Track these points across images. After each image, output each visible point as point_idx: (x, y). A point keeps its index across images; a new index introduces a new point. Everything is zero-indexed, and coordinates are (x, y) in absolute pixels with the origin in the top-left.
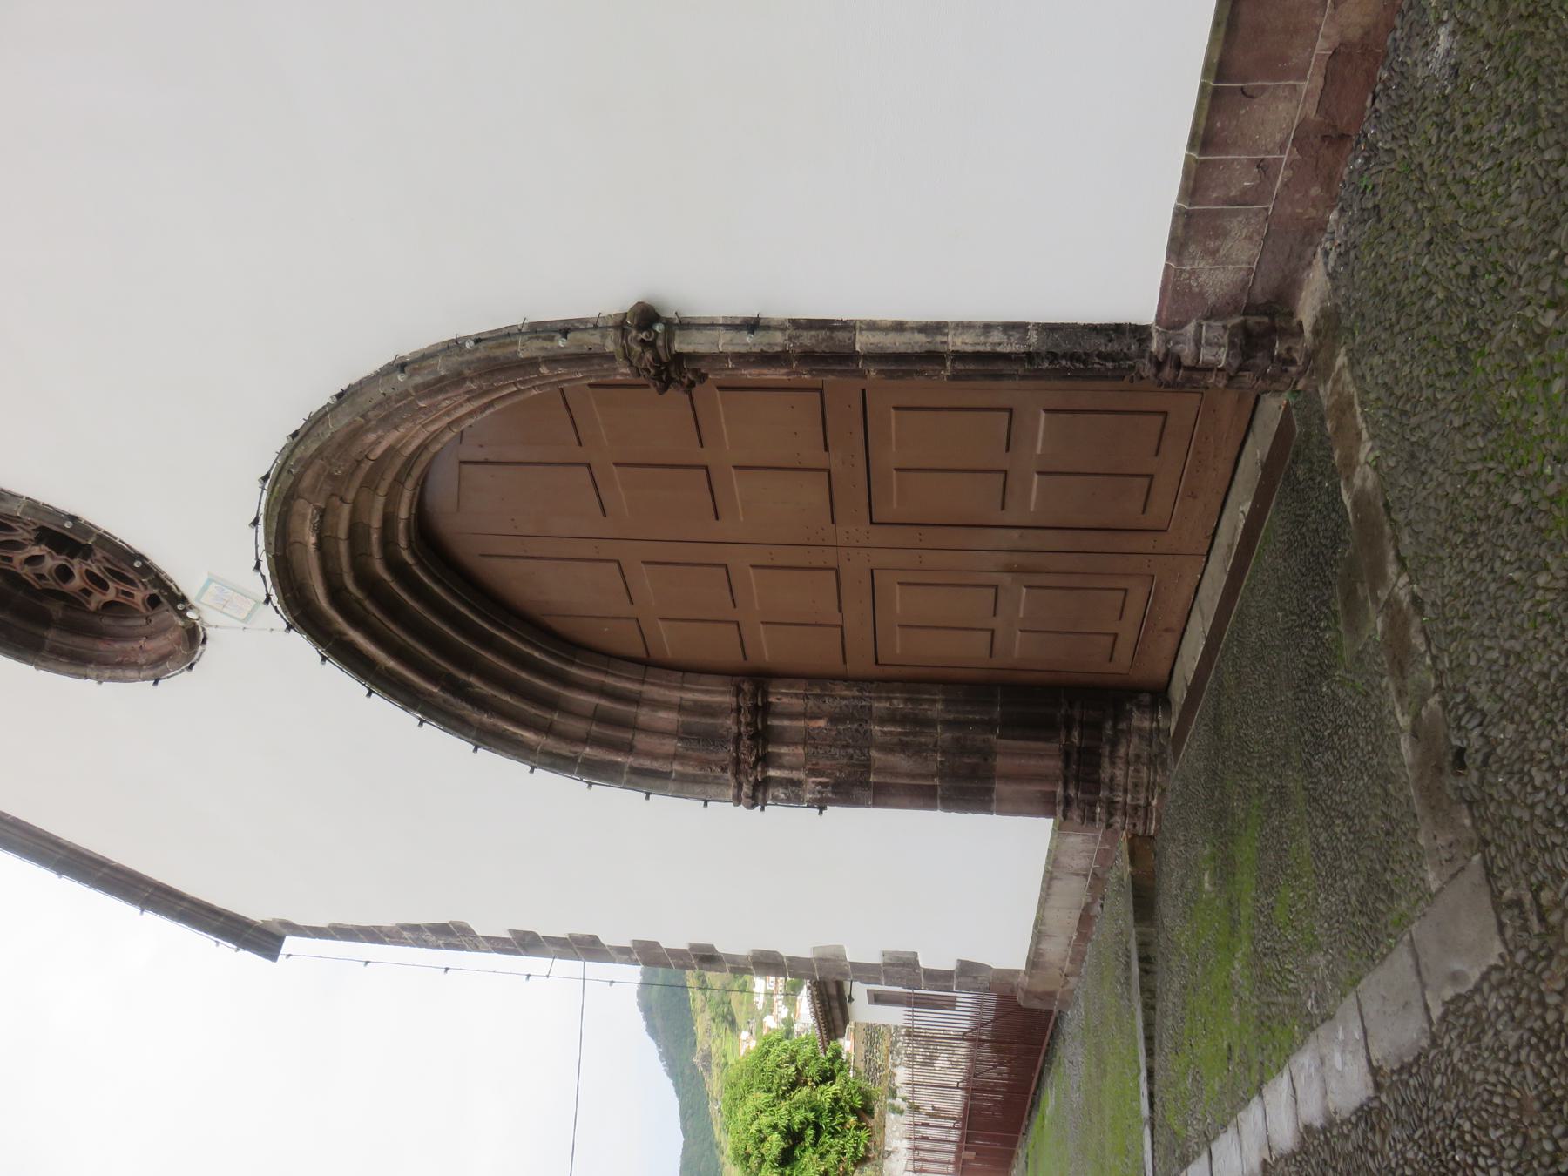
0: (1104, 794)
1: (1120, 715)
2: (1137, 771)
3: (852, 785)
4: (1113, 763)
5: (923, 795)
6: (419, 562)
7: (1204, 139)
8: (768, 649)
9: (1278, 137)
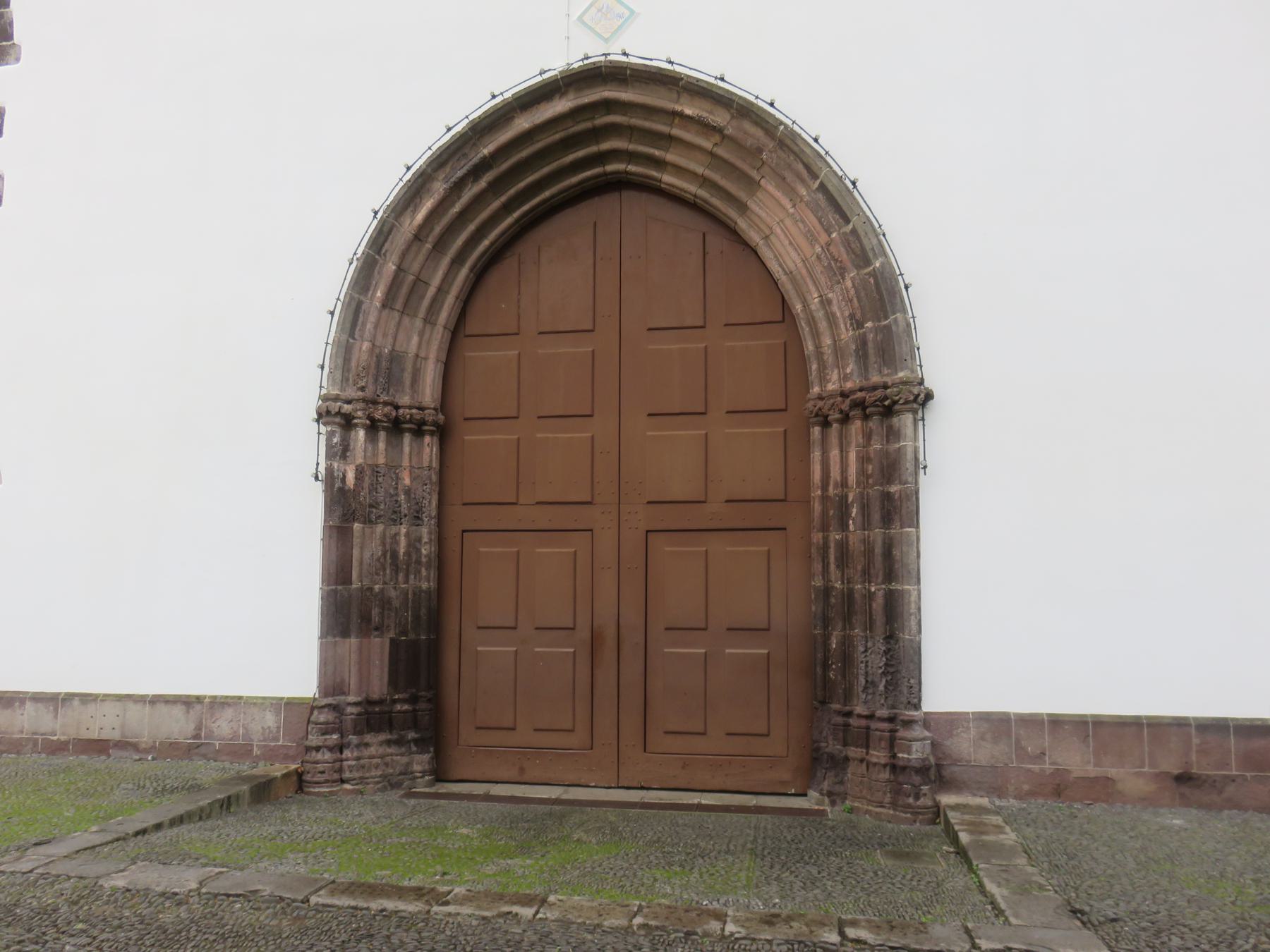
0: (354, 739)
1: (421, 744)
2: (377, 767)
3: (345, 509)
4: (381, 744)
5: (338, 572)
6: (605, 174)
8: (471, 437)
9: (1059, 760)
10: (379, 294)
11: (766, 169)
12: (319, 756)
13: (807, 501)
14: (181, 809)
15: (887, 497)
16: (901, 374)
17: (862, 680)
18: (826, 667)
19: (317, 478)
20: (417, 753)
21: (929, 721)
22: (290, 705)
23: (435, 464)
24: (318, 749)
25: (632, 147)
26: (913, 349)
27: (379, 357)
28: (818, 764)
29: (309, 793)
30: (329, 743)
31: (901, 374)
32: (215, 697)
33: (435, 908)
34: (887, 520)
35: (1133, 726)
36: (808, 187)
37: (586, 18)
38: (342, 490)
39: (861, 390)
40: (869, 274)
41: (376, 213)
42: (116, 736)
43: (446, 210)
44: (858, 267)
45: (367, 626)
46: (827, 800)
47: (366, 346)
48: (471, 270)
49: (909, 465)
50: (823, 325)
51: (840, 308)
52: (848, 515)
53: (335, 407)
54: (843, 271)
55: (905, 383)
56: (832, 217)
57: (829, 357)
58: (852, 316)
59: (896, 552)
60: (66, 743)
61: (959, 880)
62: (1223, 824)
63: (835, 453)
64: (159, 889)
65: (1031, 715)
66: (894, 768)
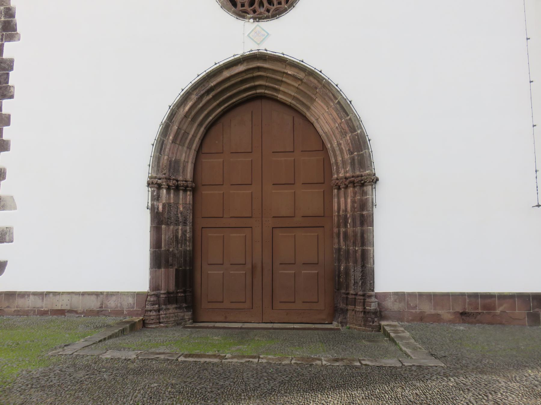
2: (172, 317)
3: (159, 220)
4: (174, 308)
6: (256, 93)
7: (421, 295)
8: (205, 192)
10: (171, 138)
11: (318, 94)
12: (151, 314)
13: (332, 217)
14: (110, 333)
15: (362, 216)
16: (367, 172)
17: (353, 281)
18: (339, 277)
19: (148, 208)
20: (187, 312)
21: (377, 295)
22: (138, 294)
23: (191, 203)
24: (150, 311)
25: (267, 84)
26: (371, 162)
27: (170, 161)
28: (336, 312)
29: (148, 328)
30: (154, 308)
31: (367, 172)
32: (108, 292)
33: (223, 360)
34: (362, 224)
35: (447, 296)
36: (333, 102)
37: (250, 35)
38: (158, 213)
39: (353, 177)
40: (355, 135)
41: (170, 107)
42: (68, 308)
43: (196, 106)
44: (352, 132)
45: (168, 265)
46: (340, 325)
47: (166, 157)
48: (205, 128)
49: (370, 204)
50: (338, 153)
51: (344, 146)
52: (348, 222)
53: (155, 181)
54: (346, 133)
55: (369, 175)
56: (342, 114)
57: (340, 165)
58: (349, 150)
59: (365, 236)
60: (48, 311)
61: (393, 348)
62: (476, 329)
63: (342, 200)
64: (124, 358)
65: (412, 293)
66: (365, 312)
